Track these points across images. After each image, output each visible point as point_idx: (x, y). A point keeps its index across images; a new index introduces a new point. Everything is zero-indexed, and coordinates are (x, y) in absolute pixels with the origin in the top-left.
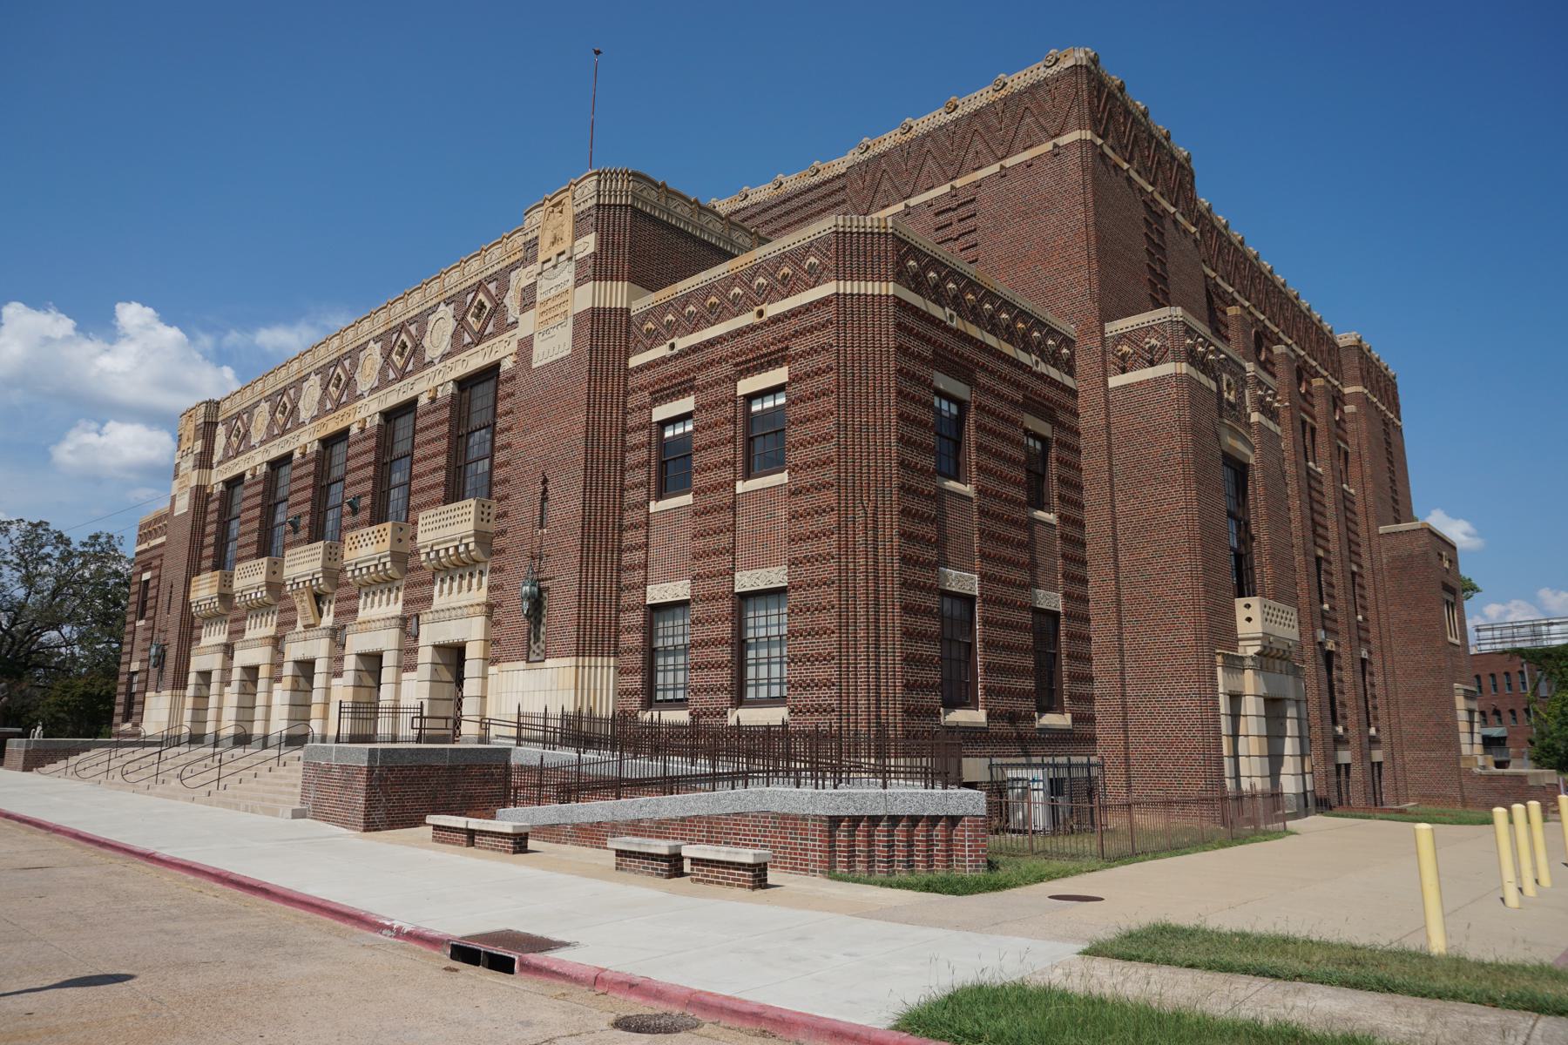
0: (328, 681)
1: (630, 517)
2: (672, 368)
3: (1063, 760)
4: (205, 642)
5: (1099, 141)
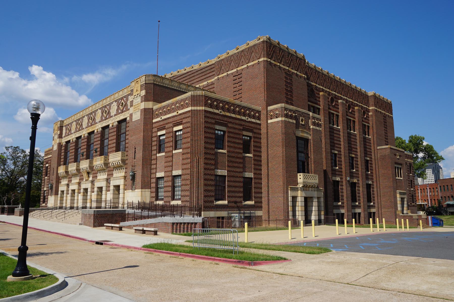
0: (91, 194)
1: (154, 157)
2: (161, 123)
3: (243, 212)
4: (62, 183)
5: (269, 60)
